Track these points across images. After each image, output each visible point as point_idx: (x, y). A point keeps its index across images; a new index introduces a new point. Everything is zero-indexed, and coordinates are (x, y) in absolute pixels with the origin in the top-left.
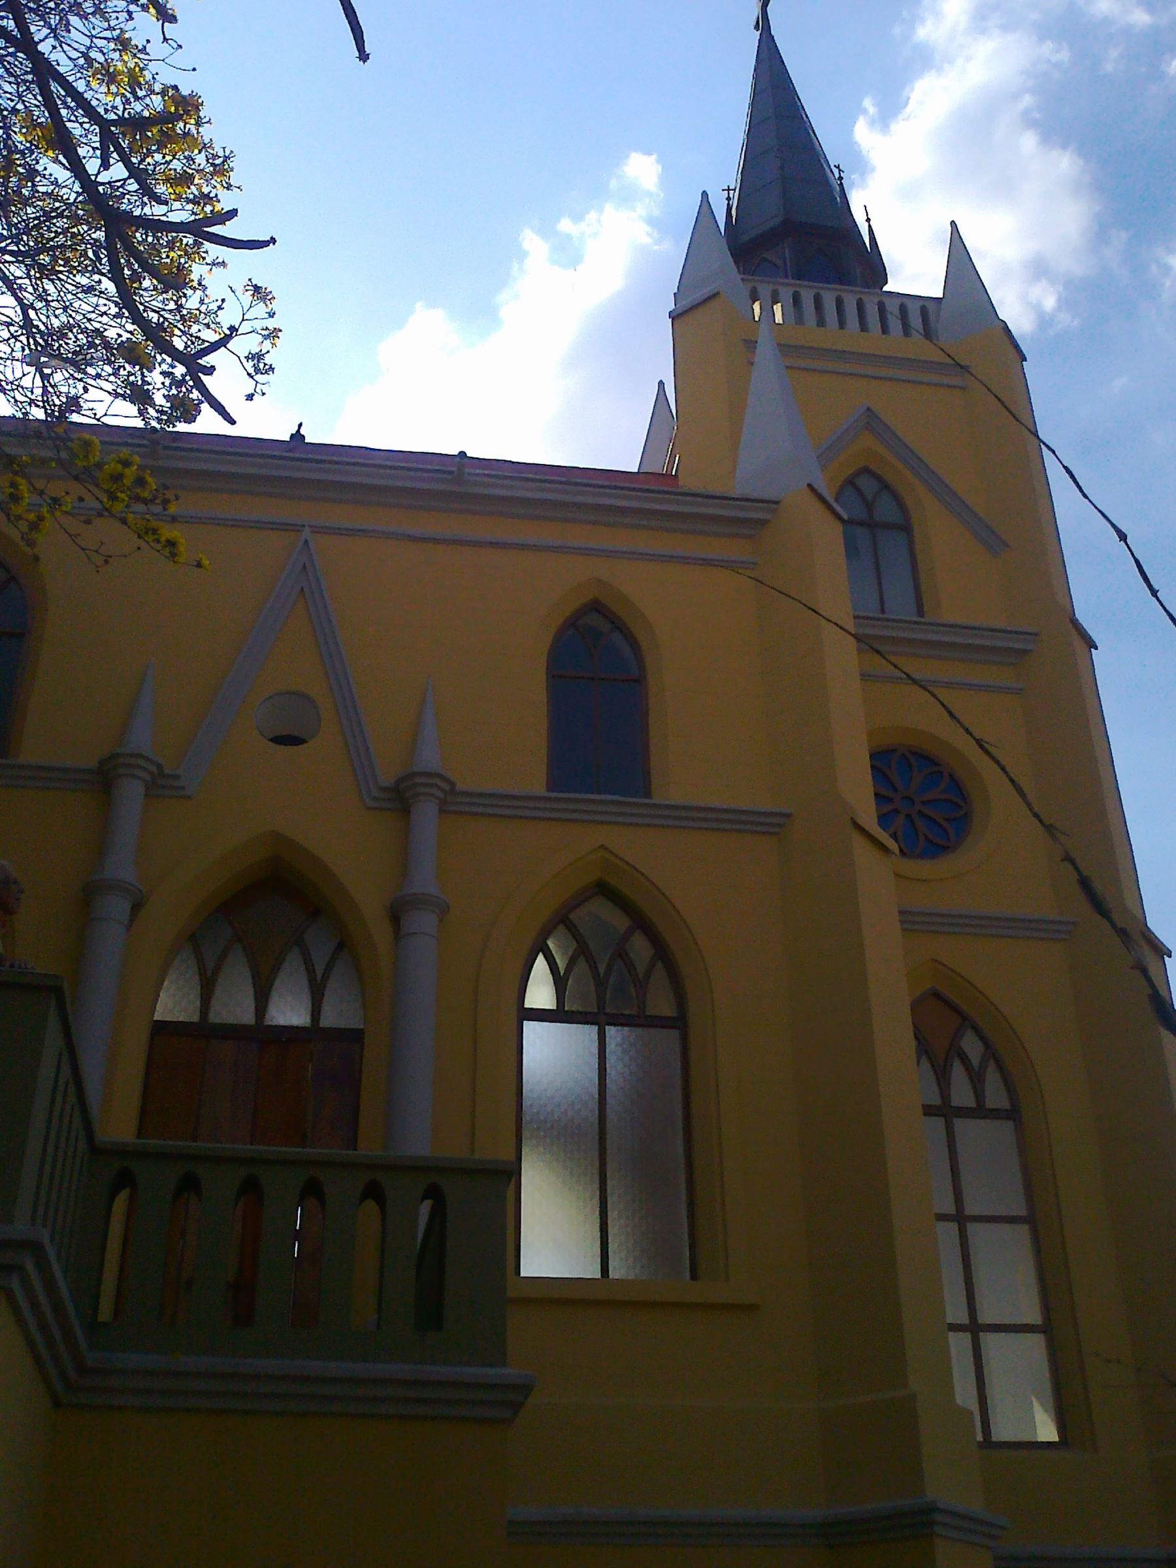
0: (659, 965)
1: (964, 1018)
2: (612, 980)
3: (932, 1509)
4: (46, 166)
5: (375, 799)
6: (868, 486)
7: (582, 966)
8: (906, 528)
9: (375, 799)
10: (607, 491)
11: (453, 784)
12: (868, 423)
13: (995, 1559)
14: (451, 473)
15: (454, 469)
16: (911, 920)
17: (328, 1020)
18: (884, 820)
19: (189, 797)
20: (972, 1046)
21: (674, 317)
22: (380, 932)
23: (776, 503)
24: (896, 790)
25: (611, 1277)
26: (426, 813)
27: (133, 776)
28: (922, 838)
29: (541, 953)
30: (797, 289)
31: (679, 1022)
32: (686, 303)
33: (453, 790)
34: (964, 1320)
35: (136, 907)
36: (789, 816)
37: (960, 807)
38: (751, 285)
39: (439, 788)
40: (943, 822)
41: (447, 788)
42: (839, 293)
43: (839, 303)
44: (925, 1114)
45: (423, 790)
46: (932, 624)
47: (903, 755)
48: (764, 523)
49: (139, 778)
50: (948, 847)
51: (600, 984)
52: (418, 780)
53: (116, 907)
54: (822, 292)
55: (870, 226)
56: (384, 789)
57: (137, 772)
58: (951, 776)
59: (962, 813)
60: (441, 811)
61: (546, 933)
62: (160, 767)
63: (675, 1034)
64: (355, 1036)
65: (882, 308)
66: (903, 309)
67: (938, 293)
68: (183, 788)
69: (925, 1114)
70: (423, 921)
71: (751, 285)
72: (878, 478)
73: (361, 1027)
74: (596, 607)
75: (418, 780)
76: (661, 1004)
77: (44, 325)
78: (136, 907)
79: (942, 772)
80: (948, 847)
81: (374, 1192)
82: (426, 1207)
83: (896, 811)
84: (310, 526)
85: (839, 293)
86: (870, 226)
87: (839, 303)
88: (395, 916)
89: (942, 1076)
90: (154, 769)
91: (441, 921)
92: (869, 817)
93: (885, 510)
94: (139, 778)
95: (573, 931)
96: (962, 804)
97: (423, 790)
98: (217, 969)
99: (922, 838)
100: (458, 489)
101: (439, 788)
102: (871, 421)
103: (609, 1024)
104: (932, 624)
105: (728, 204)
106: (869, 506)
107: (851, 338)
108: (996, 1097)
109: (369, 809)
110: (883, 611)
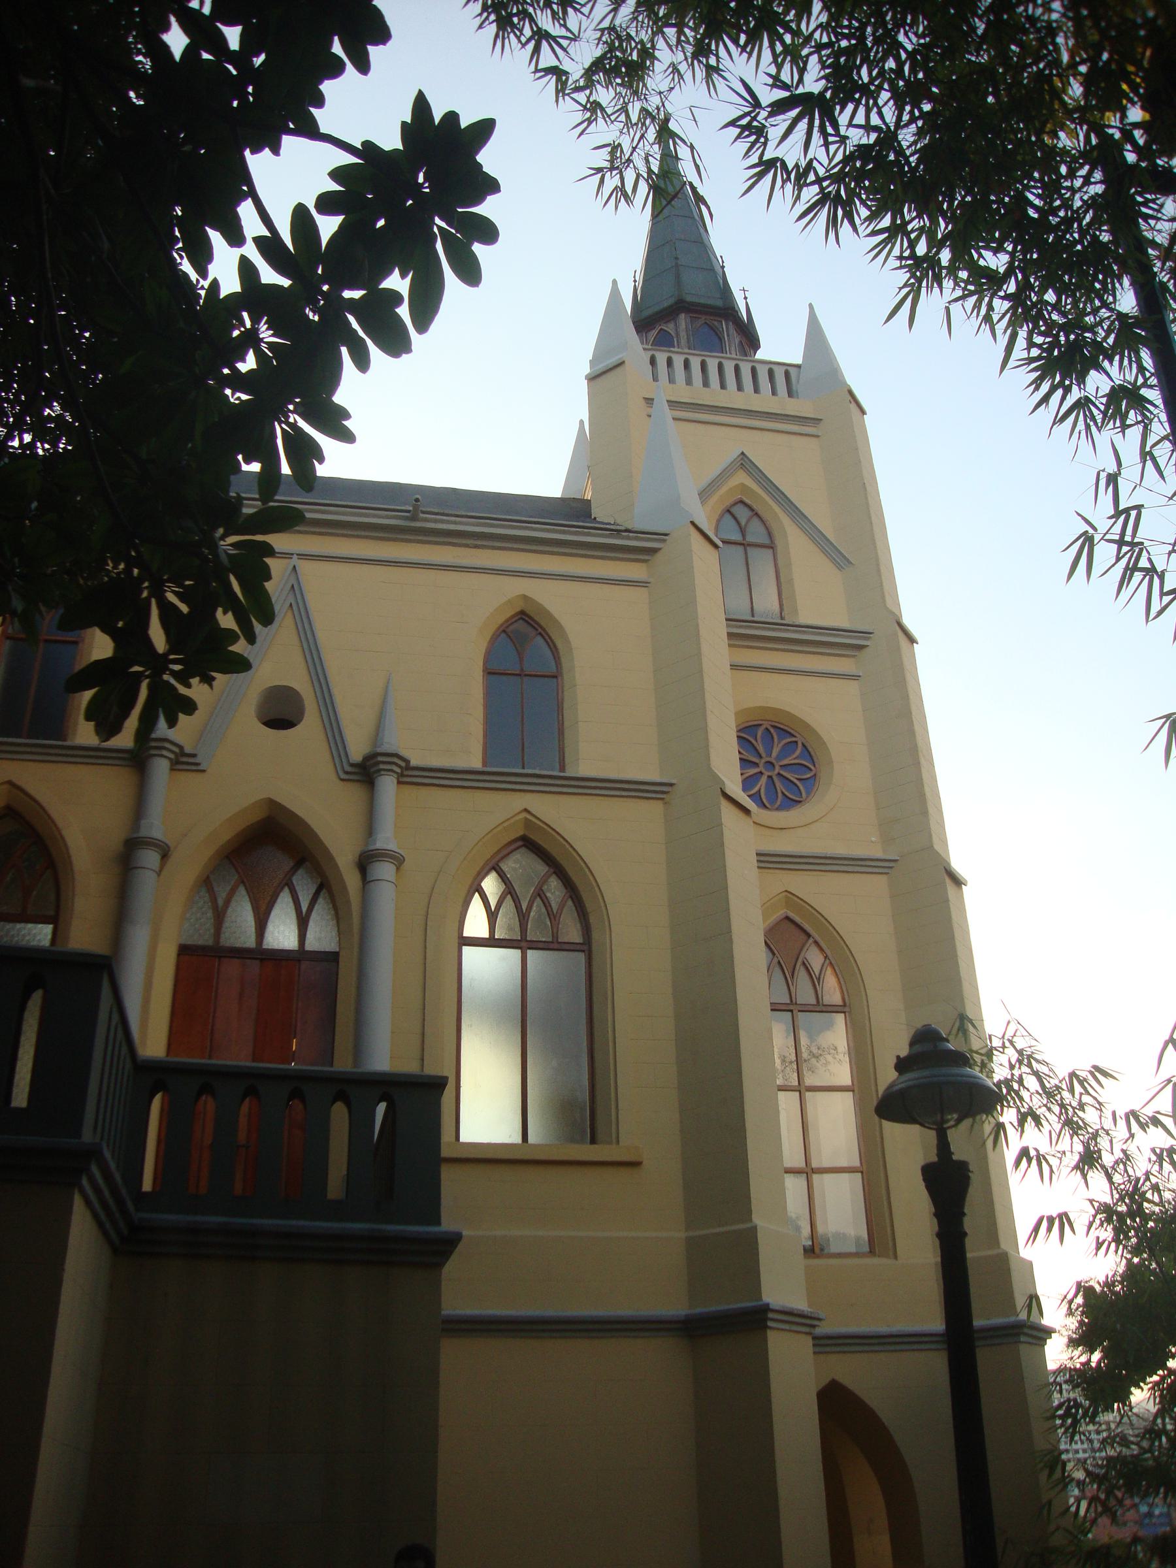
0: (570, 903)
1: (809, 935)
2: (532, 914)
3: (766, 1309)
4: (310, 726)
5: (347, 773)
6: (742, 514)
7: (509, 902)
8: (771, 546)
9: (347, 773)
10: (533, 525)
11: (407, 761)
12: (742, 464)
13: (814, 1338)
14: (408, 511)
15: (411, 508)
16: (767, 861)
17: (312, 944)
18: (747, 784)
19: (204, 771)
20: (815, 959)
21: (592, 379)
22: (351, 879)
23: (666, 535)
24: (761, 757)
25: (529, 1142)
26: (387, 785)
27: (162, 756)
28: (780, 795)
29: (477, 894)
30: (754, 364)
31: (586, 947)
32: (601, 367)
33: (408, 767)
34: (800, 1163)
35: (165, 855)
36: (671, 785)
37: (811, 770)
38: (650, 353)
39: (396, 764)
40: (796, 781)
41: (176, 750)
42: (703, 358)
43: (703, 365)
44: (772, 1010)
45: (382, 766)
46: (788, 625)
47: (767, 729)
48: (654, 551)
49: (166, 757)
50: (800, 802)
51: (523, 917)
52: (380, 759)
53: (150, 858)
54: (723, 360)
55: (747, 304)
56: (352, 765)
57: (165, 753)
58: (803, 745)
59: (812, 774)
60: (399, 783)
61: (481, 876)
62: (181, 747)
63: (581, 957)
64: (332, 958)
65: (754, 371)
66: (771, 373)
67: (798, 361)
68: (198, 764)
69: (772, 1010)
70: (384, 871)
71: (650, 353)
72: (751, 509)
73: (338, 950)
74: (522, 613)
75: (380, 759)
76: (571, 932)
77: (1040, 384)
78: (165, 855)
79: (796, 742)
80: (800, 802)
81: (342, 1096)
82: (382, 1108)
83: (761, 773)
84: (297, 555)
85: (703, 358)
86: (747, 304)
87: (703, 365)
88: (365, 863)
89: (789, 978)
90: (176, 750)
91: (398, 869)
92: (735, 788)
93: (756, 533)
94: (166, 757)
95: (502, 876)
96: (812, 768)
97: (382, 766)
98: (228, 902)
99: (780, 795)
100: (414, 524)
101: (396, 764)
102: (744, 462)
103: (530, 948)
104: (788, 625)
105: (635, 285)
106: (743, 532)
107: (731, 397)
108: (832, 992)
109: (342, 780)
110: (753, 616)
